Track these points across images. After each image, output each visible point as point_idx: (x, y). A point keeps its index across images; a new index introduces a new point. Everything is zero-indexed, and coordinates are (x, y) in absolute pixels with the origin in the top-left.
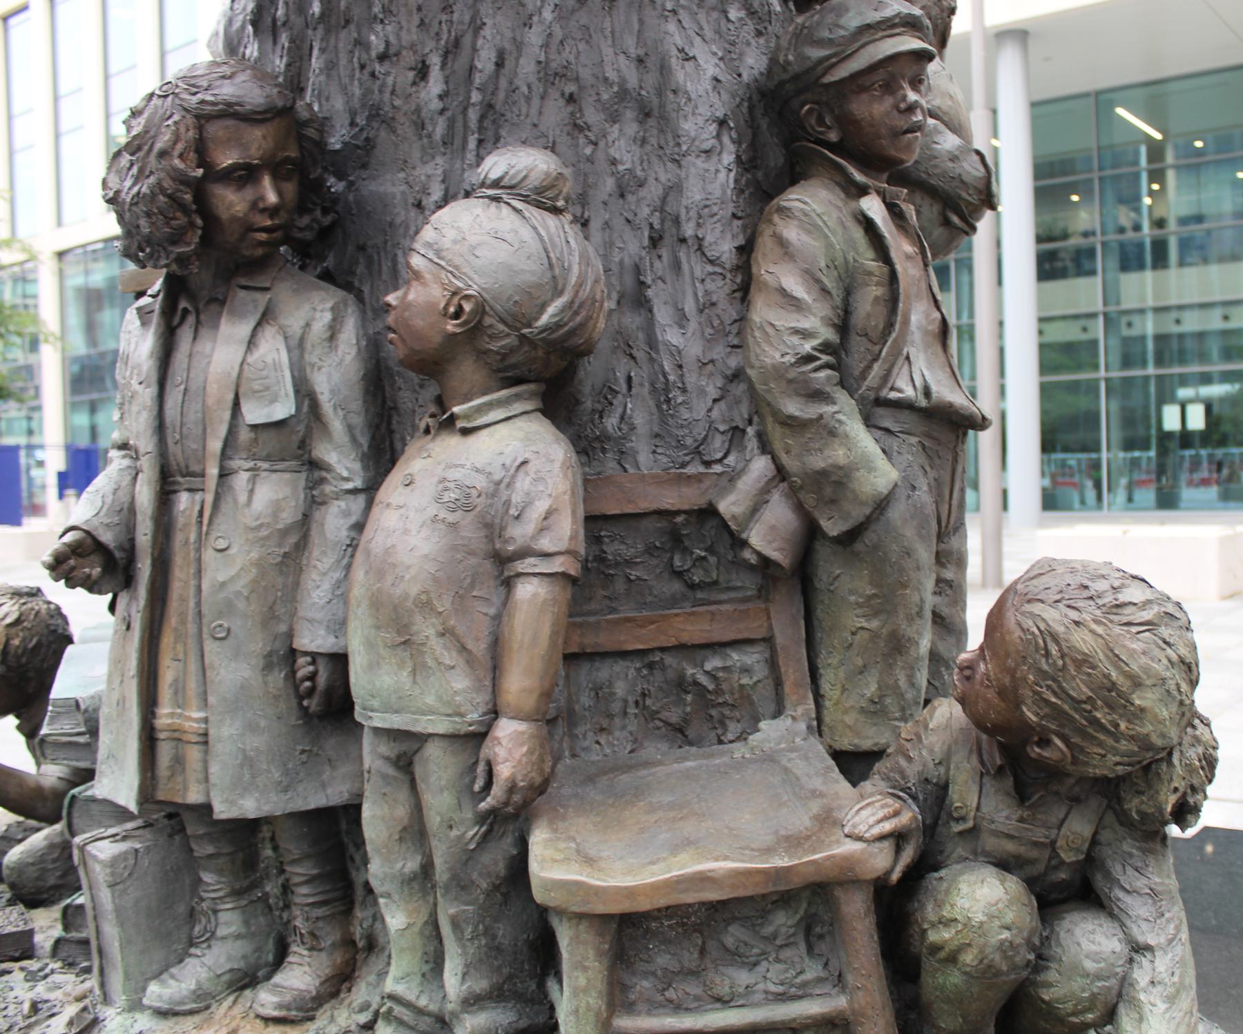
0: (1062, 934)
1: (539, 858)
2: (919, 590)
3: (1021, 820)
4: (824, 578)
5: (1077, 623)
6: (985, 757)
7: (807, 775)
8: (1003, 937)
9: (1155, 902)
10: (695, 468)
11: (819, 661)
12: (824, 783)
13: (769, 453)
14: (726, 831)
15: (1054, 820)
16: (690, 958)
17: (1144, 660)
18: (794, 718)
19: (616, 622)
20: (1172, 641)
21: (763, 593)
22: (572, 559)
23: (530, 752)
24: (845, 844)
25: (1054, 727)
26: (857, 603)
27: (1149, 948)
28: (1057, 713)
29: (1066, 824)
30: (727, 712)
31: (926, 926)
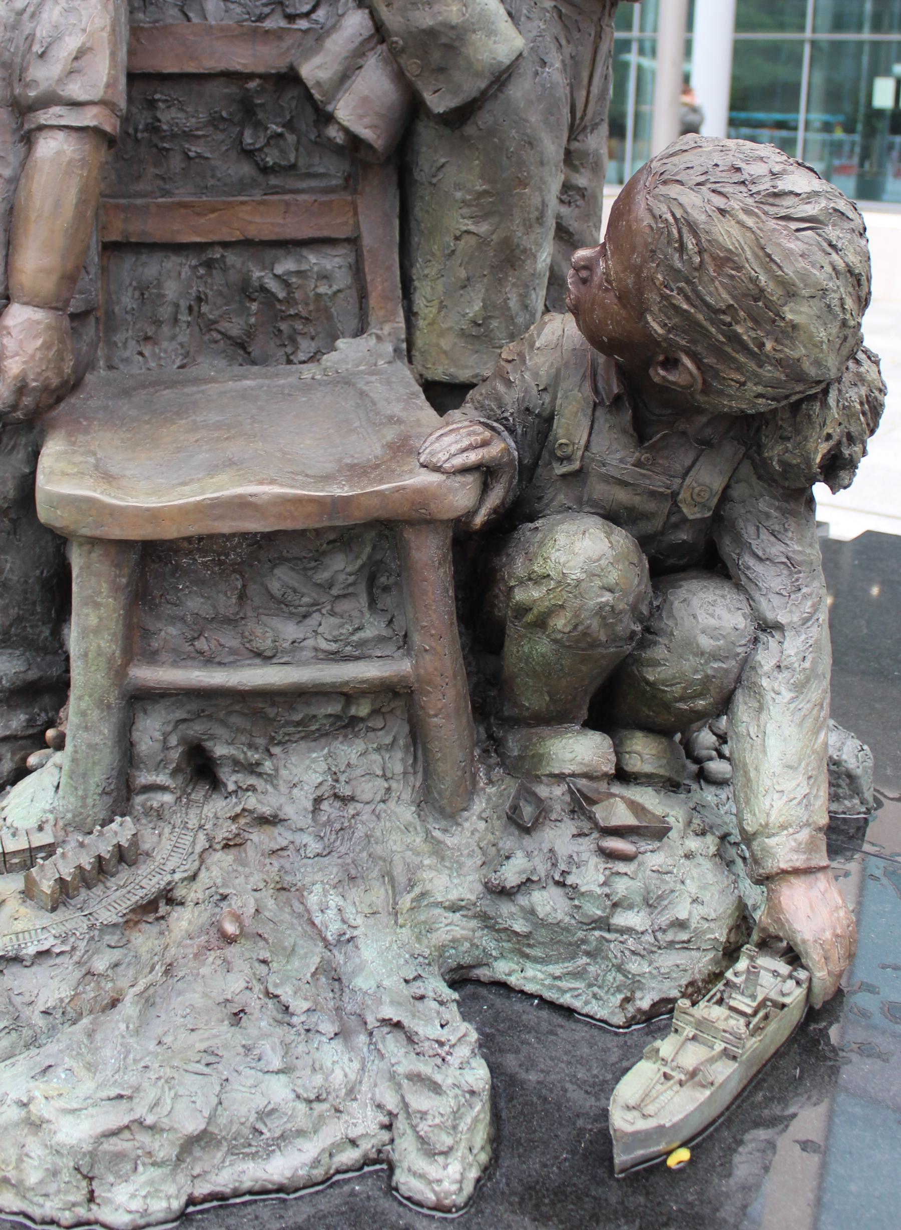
0: (676, 604)
1: (47, 470)
2: (541, 190)
3: (638, 464)
4: (426, 168)
5: (722, 212)
6: (600, 385)
7: (386, 400)
8: (603, 599)
9: (791, 574)
10: (275, 22)
11: (414, 271)
12: (404, 409)
13: (367, 7)
14: (279, 454)
15: (678, 467)
16: (227, 603)
17: (802, 264)
18: (379, 338)
19: (170, 207)
20: (839, 245)
21: (350, 184)
22: (107, 112)
23: (46, 346)
24: (419, 475)
25: (684, 343)
26: (463, 201)
27: (778, 627)
28: (689, 324)
29: (692, 473)
30: (299, 326)
31: (512, 583)
